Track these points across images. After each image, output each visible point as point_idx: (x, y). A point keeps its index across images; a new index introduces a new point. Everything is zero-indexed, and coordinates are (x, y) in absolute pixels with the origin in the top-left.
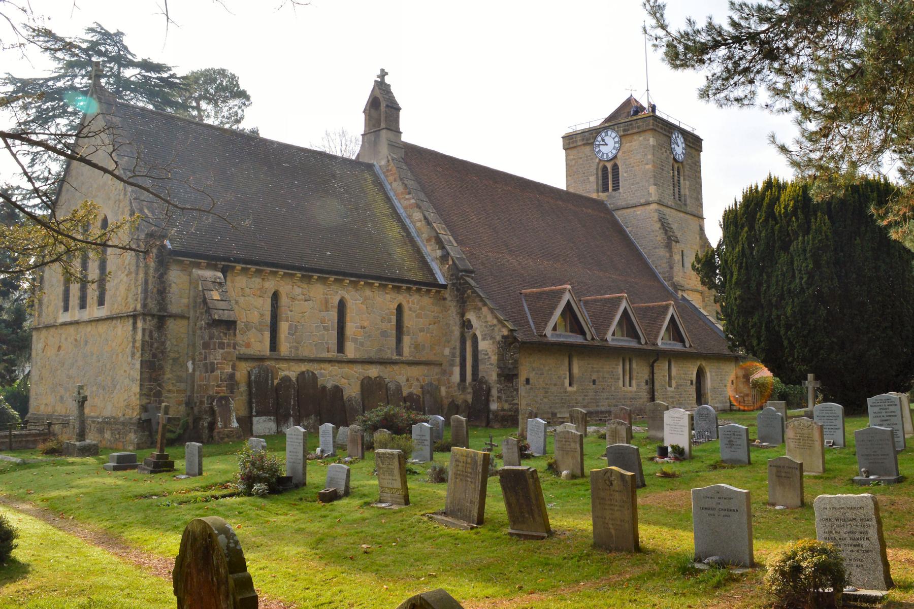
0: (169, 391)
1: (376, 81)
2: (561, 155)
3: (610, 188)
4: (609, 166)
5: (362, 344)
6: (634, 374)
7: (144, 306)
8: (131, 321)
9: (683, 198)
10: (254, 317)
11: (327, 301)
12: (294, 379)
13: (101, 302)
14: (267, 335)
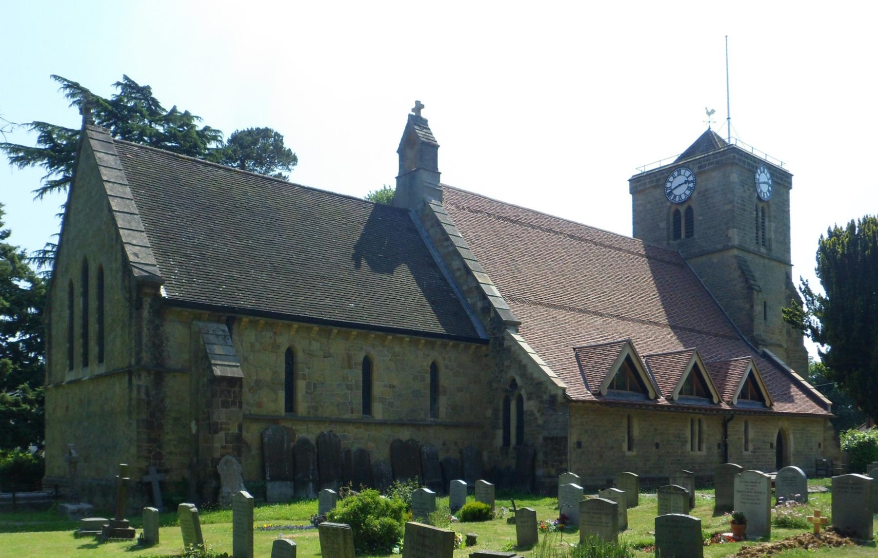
0: (171, 453)
1: (410, 115)
3: (683, 236)
6: (705, 436)
7: (139, 361)
8: (127, 378)
9: (767, 243)
11: (349, 358)
12: (313, 442)
13: (101, 359)
14: (282, 394)
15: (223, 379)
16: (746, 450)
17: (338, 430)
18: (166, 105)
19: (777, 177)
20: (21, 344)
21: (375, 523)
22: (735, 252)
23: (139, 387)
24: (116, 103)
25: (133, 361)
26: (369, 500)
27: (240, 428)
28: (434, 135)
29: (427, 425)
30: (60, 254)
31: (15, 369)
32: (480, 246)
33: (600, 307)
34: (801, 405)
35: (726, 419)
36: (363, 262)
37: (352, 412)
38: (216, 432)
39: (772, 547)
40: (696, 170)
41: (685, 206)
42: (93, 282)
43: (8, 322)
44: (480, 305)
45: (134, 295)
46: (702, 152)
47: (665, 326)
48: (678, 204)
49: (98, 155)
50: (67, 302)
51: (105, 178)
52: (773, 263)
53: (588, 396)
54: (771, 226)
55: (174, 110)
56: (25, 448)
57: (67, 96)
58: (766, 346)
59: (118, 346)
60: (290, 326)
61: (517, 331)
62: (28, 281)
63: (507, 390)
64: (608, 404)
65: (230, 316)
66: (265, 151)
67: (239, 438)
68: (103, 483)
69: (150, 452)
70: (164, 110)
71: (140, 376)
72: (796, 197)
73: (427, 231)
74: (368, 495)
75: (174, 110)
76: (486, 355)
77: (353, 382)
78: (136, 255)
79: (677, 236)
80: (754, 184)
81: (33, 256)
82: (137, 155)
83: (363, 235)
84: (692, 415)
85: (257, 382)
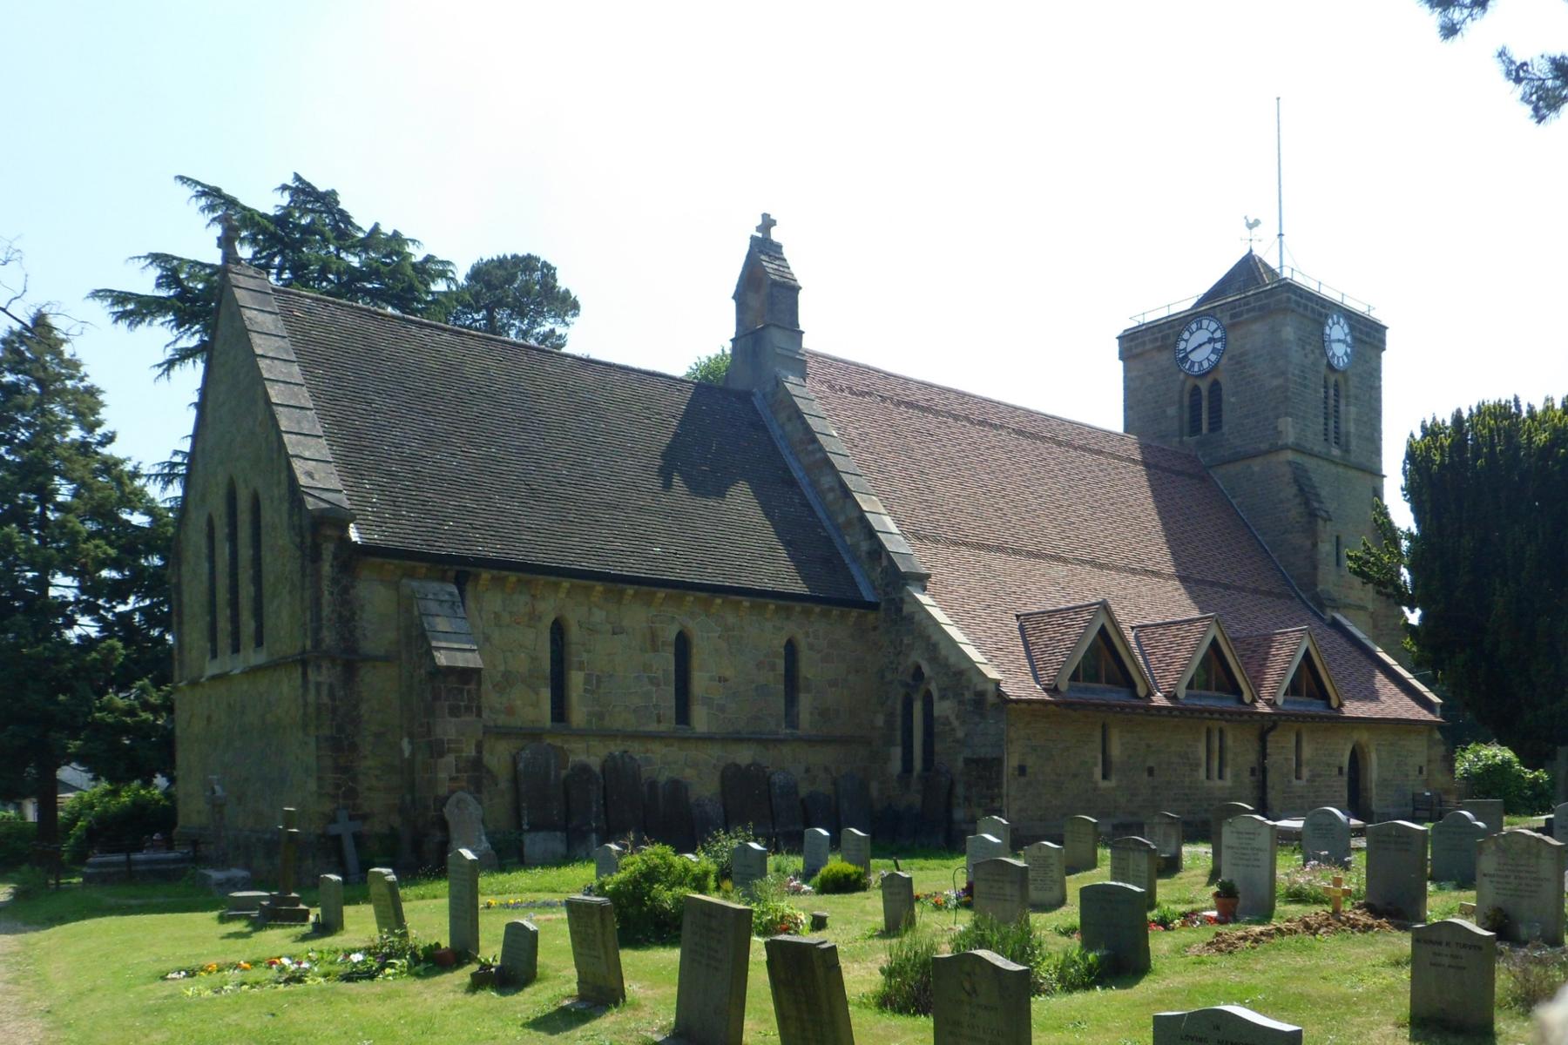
0: (370, 789)
1: (753, 238)
2: (1115, 371)
4: (1204, 386)
5: (722, 709)
6: (1229, 756)
7: (317, 643)
9: (1343, 439)
10: (520, 664)
11: (654, 637)
12: (597, 769)
13: (259, 641)
14: (546, 694)
15: (451, 670)
16: (1298, 777)
17: (636, 749)
18: (363, 220)
19: (1361, 332)
20: (137, 617)
21: (666, 896)
22: (1289, 455)
23: (318, 685)
24: (282, 220)
25: (309, 644)
26: (658, 861)
27: (479, 747)
28: (793, 269)
29: (781, 741)
30: (194, 467)
31: (127, 656)
32: (866, 449)
33: (1062, 547)
34: (1393, 704)
35: (1265, 728)
36: (677, 480)
37: (659, 721)
38: (441, 755)
39: (1262, 933)
40: (1226, 321)
41: (1210, 379)
42: (244, 518)
43: (113, 580)
44: (865, 546)
45: (308, 540)
46: (1239, 291)
47: (1170, 577)
48: (1197, 377)
49: (247, 313)
50: (205, 550)
51: (259, 351)
52: (1352, 473)
53: (1036, 692)
54: (1350, 412)
55: (376, 229)
56: (148, 783)
57: (202, 210)
58: (1337, 608)
59: (285, 621)
60: (557, 586)
61: (924, 589)
62: (144, 514)
63: (907, 685)
64: (1069, 705)
65: (461, 571)
66: (528, 293)
67: (477, 764)
68: (268, 836)
69: (338, 786)
70: (360, 229)
71: (319, 667)
72: (1392, 363)
73: (782, 427)
74: (655, 853)
75: (376, 229)
76: (875, 628)
77: (660, 674)
78: (310, 475)
79: (1195, 427)
80: (1323, 343)
81: (153, 471)
82: (309, 312)
83: (676, 434)
84: (1210, 723)
85: (507, 675)
